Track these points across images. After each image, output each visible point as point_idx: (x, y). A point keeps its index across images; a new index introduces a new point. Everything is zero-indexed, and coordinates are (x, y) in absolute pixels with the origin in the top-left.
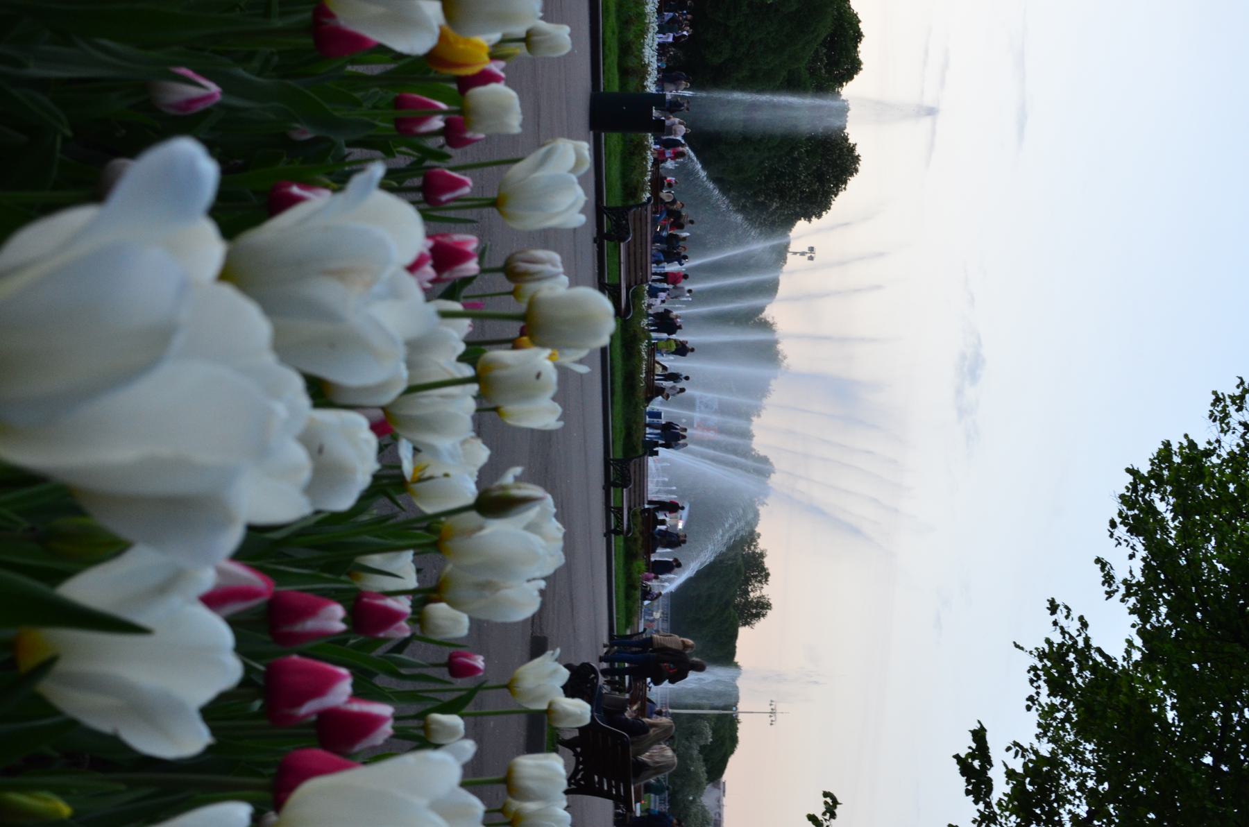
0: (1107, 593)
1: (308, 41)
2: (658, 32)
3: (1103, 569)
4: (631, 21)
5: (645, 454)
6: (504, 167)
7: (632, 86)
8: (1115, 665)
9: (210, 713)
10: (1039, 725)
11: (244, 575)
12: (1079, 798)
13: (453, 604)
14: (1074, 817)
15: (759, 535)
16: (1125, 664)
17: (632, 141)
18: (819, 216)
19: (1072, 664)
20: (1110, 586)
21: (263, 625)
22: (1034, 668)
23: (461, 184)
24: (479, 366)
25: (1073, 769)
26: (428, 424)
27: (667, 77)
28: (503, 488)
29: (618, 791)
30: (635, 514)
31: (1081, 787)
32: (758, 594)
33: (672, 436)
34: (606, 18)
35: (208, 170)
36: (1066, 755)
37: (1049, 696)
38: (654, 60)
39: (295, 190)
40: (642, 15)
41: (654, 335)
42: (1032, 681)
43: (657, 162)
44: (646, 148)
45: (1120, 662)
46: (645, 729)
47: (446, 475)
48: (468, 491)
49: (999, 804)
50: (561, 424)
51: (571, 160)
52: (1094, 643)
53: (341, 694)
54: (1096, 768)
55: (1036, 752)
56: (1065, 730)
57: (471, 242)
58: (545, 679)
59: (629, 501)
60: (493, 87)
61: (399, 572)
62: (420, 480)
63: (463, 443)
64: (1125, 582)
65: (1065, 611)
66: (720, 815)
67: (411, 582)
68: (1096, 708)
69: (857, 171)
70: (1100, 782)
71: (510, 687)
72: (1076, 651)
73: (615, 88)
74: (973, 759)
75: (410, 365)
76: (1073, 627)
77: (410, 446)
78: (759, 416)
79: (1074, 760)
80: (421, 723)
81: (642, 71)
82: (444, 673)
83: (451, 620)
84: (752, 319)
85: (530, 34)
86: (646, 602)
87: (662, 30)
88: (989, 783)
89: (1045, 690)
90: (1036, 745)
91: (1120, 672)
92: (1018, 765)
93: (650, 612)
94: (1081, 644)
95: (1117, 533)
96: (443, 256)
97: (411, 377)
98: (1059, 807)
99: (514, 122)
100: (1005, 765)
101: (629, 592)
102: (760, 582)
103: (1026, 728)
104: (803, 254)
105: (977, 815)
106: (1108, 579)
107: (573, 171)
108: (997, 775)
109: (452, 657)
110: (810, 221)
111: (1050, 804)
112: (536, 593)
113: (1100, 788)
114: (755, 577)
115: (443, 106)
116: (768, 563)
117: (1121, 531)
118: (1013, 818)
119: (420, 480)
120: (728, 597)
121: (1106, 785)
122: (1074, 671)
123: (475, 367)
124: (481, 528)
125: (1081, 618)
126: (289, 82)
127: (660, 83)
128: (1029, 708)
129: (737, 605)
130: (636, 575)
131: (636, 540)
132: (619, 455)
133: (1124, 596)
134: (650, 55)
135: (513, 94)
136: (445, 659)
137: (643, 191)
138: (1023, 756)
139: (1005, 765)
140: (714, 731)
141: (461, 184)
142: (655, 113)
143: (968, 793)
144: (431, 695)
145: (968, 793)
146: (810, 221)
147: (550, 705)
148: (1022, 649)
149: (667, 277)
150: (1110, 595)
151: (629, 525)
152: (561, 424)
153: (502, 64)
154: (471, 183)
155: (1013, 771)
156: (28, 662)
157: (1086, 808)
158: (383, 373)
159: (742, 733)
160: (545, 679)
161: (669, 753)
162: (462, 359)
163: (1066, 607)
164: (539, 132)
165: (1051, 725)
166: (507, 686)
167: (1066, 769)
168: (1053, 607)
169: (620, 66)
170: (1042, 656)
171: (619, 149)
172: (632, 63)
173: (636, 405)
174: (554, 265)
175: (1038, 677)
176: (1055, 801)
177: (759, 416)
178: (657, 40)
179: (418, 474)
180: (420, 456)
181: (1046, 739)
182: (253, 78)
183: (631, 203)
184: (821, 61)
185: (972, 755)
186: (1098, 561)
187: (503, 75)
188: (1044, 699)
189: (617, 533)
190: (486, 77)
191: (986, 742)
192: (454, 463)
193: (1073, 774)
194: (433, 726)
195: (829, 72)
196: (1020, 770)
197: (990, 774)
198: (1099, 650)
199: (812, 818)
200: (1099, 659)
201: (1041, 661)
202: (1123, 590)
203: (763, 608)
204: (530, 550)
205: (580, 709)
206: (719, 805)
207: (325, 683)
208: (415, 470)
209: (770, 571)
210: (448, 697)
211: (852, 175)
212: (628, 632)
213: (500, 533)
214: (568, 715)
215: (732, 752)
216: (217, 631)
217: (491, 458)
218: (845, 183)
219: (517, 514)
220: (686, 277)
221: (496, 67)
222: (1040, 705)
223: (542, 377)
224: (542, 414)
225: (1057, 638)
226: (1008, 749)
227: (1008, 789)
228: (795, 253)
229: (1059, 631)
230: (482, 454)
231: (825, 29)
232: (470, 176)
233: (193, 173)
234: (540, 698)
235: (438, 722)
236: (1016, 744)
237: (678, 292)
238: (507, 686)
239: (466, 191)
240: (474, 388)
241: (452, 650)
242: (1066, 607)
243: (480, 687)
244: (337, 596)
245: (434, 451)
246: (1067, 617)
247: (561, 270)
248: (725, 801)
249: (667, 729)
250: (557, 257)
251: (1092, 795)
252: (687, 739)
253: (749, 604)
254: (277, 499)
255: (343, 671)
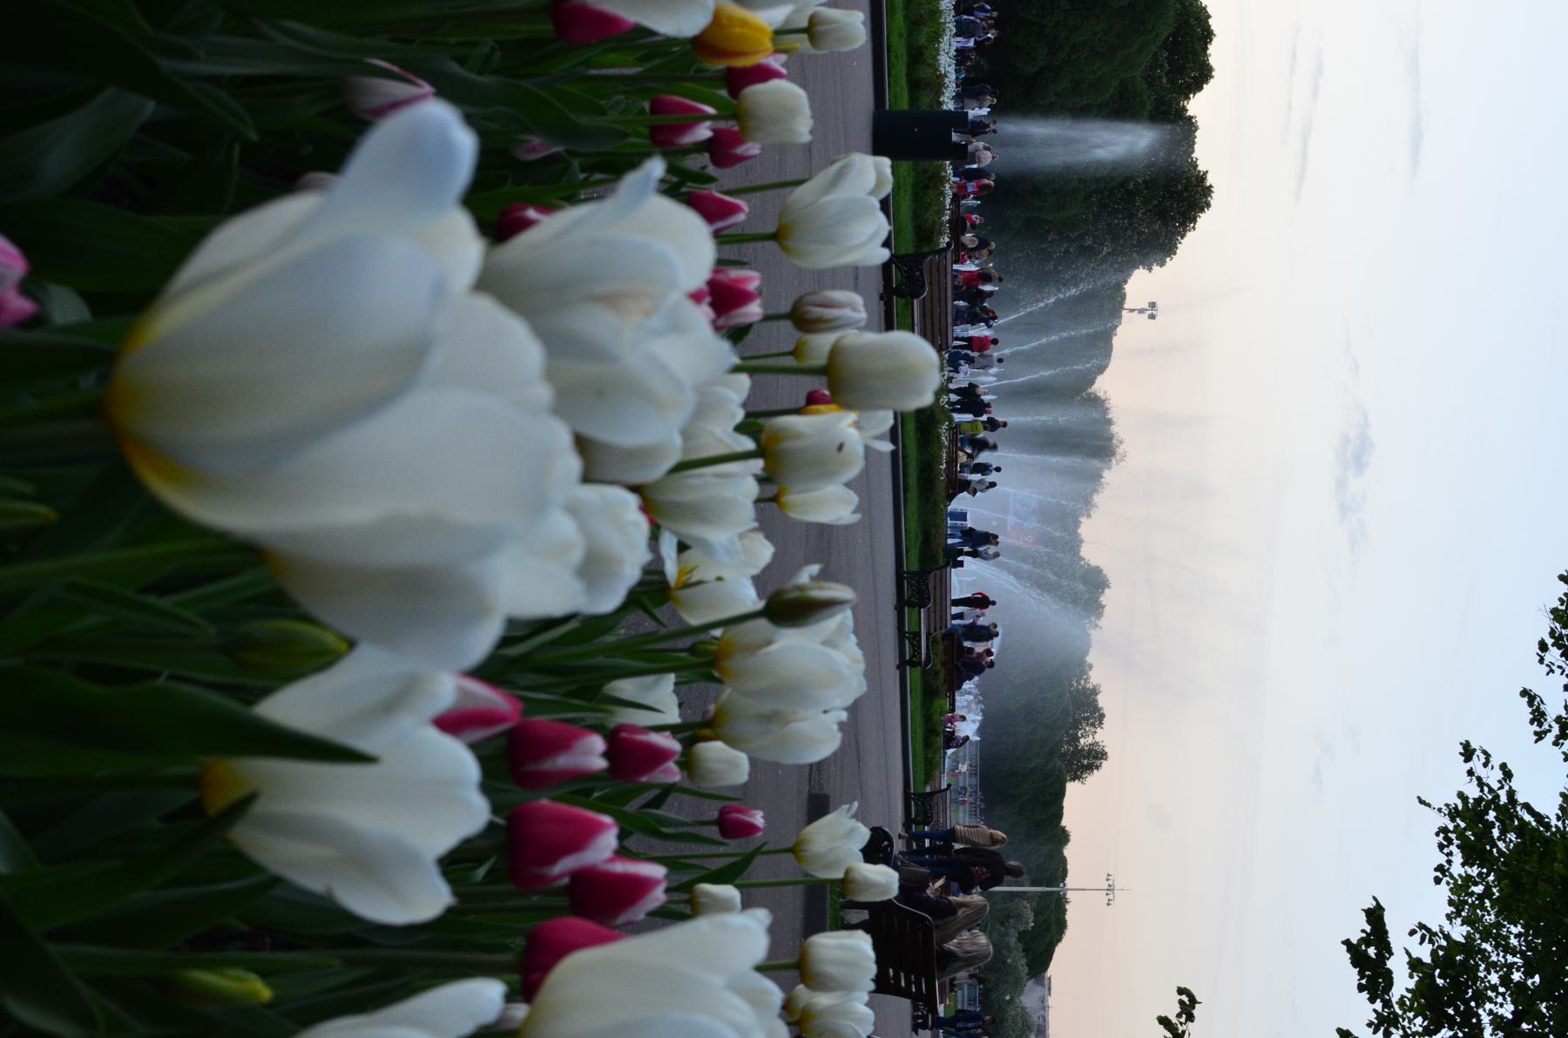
0: (1536, 733)
1: (546, 28)
2: (957, 35)
3: (1530, 703)
4: (922, 20)
5: (947, 564)
6: (788, 190)
7: (925, 102)
8: (1548, 826)
9: (454, 864)
10: (1451, 902)
11: (487, 696)
12: (1503, 995)
13: (732, 742)
14: (1498, 1022)
15: (1091, 667)
16: (1560, 824)
17: (925, 171)
18: (1162, 264)
19: (1492, 825)
20: (1540, 725)
21: (511, 759)
22: (1443, 830)
23: (734, 209)
24: (764, 437)
25: (1494, 958)
26: (699, 512)
27: (967, 91)
28: (801, 588)
29: (919, 988)
30: (935, 641)
31: (1505, 980)
32: (1090, 740)
33: (978, 542)
34: (891, 15)
35: (465, 143)
36: (1484, 940)
37: (1463, 865)
38: (952, 69)
39: (531, 213)
40: (936, 13)
41: (958, 417)
42: (1441, 847)
43: (956, 198)
44: (943, 180)
45: (1554, 822)
46: (952, 909)
47: (719, 579)
48: (749, 599)
49: (1401, 1002)
50: (858, 517)
51: (870, 180)
52: (1521, 798)
53: (603, 849)
54: (1523, 954)
55: (1447, 937)
56: (1483, 909)
57: (752, 279)
58: (839, 840)
59: (928, 625)
60: (775, 83)
61: (656, 702)
62: (687, 585)
63: (741, 536)
64: (1558, 719)
65: (1483, 757)
66: (1045, 1019)
67: (673, 716)
68: (1524, 880)
69: (1208, 205)
70: (1529, 974)
71: (795, 850)
72: (1498, 808)
73: (904, 104)
74: (1368, 946)
75: (686, 434)
76: (1493, 777)
77: (675, 541)
78: (1089, 516)
79: (1496, 947)
80: (685, 896)
81: (937, 83)
82: (713, 832)
83: (727, 762)
84: (1078, 391)
85: (813, 20)
86: (950, 752)
87: (963, 30)
88: (1388, 977)
89: (1458, 858)
90: (1447, 928)
91: (1554, 834)
92: (1424, 953)
93: (956, 762)
94: (1503, 799)
95: (1548, 657)
96: (722, 296)
97: (685, 450)
98: (1478, 1006)
99: (803, 128)
100: (1407, 952)
101: (929, 735)
102: (1093, 725)
103: (1435, 907)
104: (1142, 311)
105: (1373, 1017)
106: (1538, 716)
107: (872, 193)
108: (1398, 965)
109: (723, 813)
110: (1150, 270)
111: (1466, 1002)
112: (835, 727)
113: (1529, 982)
114: (1087, 719)
115: (710, 110)
116: (1102, 701)
117: (1554, 654)
118: (1419, 1020)
119: (687, 585)
120: (1042, 757)
121: (1537, 979)
122: (1496, 833)
123: (757, 440)
124: (769, 642)
125: (1503, 766)
126: (523, 83)
127: (958, 98)
128: (1438, 881)
129: (1065, 754)
130: (936, 717)
131: (936, 673)
132: (915, 567)
133: (1558, 738)
134: (946, 63)
135: (801, 92)
136: (715, 814)
137: (940, 234)
138: (1431, 941)
139: (1407, 952)
140: (1037, 913)
141: (734, 209)
142: (955, 137)
143: (1361, 988)
144: (694, 861)
145: (1361, 988)
146: (1150, 270)
147: (847, 872)
148: (1429, 805)
149: (972, 343)
150: (1540, 736)
151: (928, 654)
152: (858, 517)
153: (783, 57)
154: (746, 209)
155: (1419, 960)
156: (217, 802)
157: (1512, 1008)
158: (657, 434)
159: (1072, 915)
160: (839, 840)
161: (983, 939)
162: (740, 429)
163: (1485, 752)
164: (822, 153)
165: (1466, 902)
166: (791, 850)
167: (1485, 957)
168: (1468, 752)
169: (909, 76)
170: (1454, 814)
171: (910, 181)
172: (924, 73)
173: (936, 503)
174: (855, 310)
175: (1450, 842)
176: (1472, 998)
177: (1089, 516)
178: (955, 45)
179: (684, 578)
180: (687, 554)
181: (1459, 920)
182: (473, 76)
183: (926, 249)
184: (1162, 67)
185: (1366, 941)
186: (1524, 693)
187: (784, 71)
188: (1457, 869)
189: (913, 664)
190: (764, 74)
191: (1384, 924)
192: (731, 565)
193: (1494, 965)
194: (703, 900)
195: (1172, 81)
196: (1427, 959)
197: (1390, 964)
198: (1527, 806)
199: (1164, 1021)
200: (1527, 818)
201: (1453, 820)
202: (1556, 730)
203: (1096, 758)
204: (830, 672)
205: (883, 879)
206: (1044, 1007)
207: (584, 835)
208: (680, 573)
209: (1105, 711)
210: (716, 864)
211: (1202, 210)
212: (928, 789)
213: (794, 647)
214: (870, 885)
215: (1059, 940)
216: (459, 761)
217: (775, 555)
218: (1194, 220)
219: (819, 621)
220: (995, 342)
221: (776, 62)
222: (1452, 877)
223: (845, 449)
224: (831, 503)
225: (1473, 792)
226: (1412, 933)
227: (1412, 984)
228: (1132, 310)
229: (1475, 782)
230: (764, 552)
231: (1165, 28)
232: (749, 202)
233: (446, 147)
234: (830, 866)
235: (708, 894)
236: (1422, 926)
237: (983, 362)
238: (791, 850)
239: (741, 217)
240: (757, 465)
241: (727, 803)
242: (1485, 752)
243: (758, 851)
244: (597, 728)
245: (706, 546)
246: (1485, 765)
247: (863, 315)
248: (1051, 1001)
249: (980, 910)
250: (858, 300)
251: (1519, 993)
252: (1002, 924)
253: (1079, 753)
254: (535, 582)
255: (607, 819)
